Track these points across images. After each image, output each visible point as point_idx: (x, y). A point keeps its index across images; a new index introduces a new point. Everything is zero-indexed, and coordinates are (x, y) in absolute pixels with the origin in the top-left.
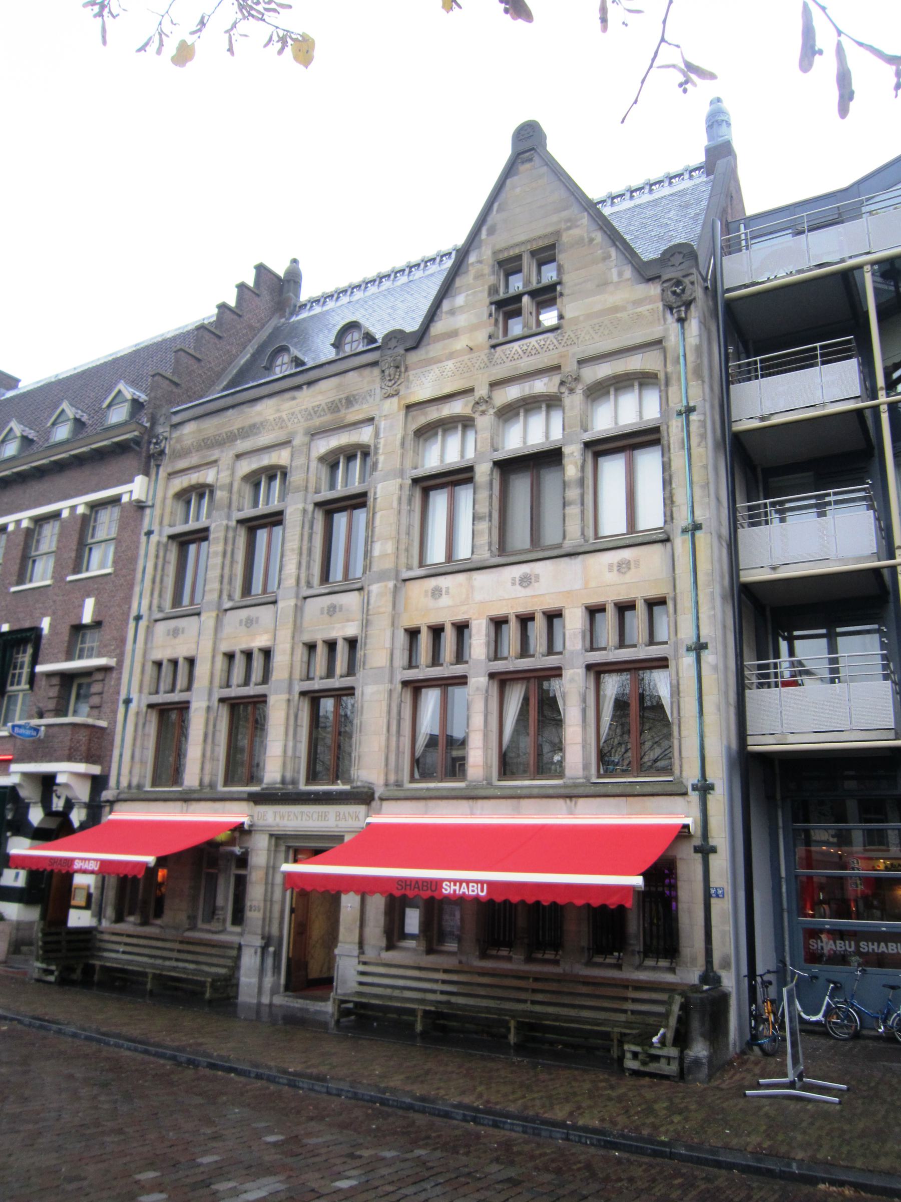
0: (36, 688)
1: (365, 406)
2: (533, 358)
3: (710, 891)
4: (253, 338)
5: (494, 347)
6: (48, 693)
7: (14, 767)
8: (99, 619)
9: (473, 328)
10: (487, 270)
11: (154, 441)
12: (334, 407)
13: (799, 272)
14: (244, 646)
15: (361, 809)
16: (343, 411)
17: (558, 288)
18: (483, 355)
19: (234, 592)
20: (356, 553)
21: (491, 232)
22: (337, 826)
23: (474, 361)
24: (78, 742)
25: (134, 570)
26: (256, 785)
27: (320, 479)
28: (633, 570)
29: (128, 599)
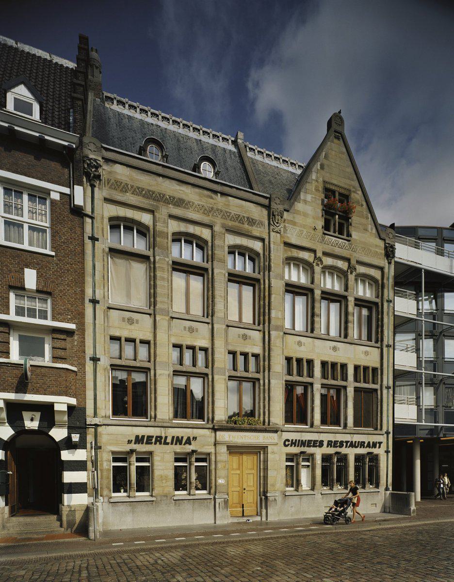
2: (340, 249)
10: (67, 65)
13: (408, 261)
20: (300, 322)
29: (81, 283)
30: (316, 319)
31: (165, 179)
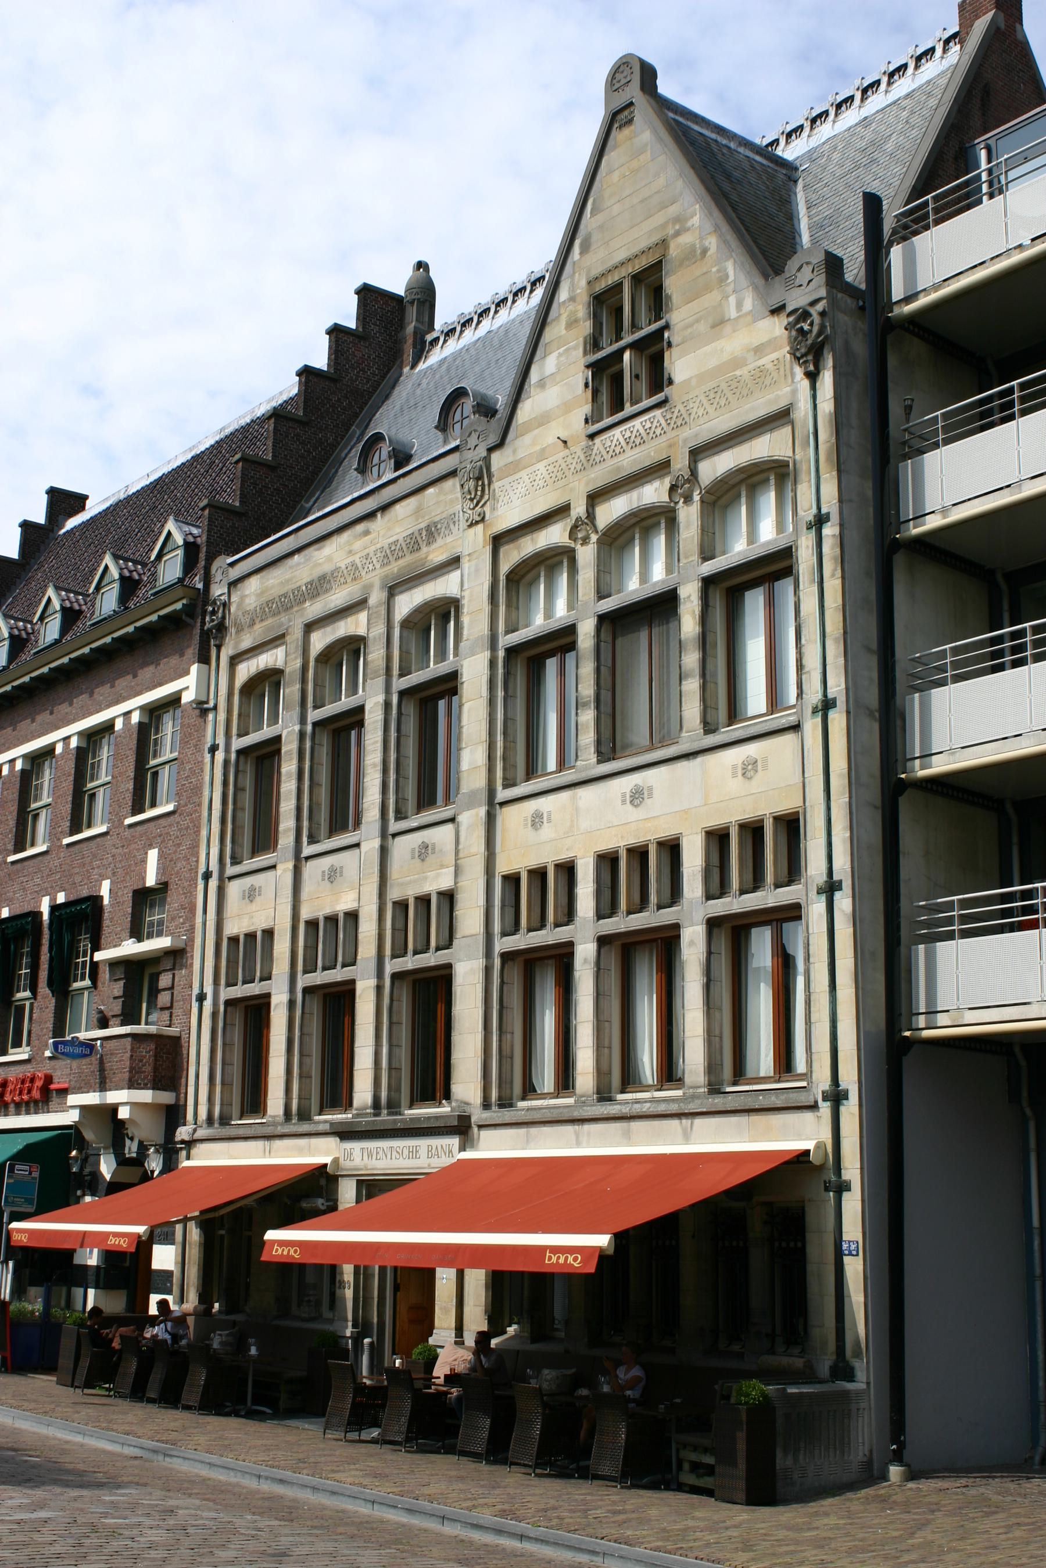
0: (100, 984)
1: (449, 539)
3: (841, 1246)
4: (361, 409)
5: (592, 436)
6: (113, 988)
7: (73, 1099)
8: (164, 879)
9: (567, 408)
11: (210, 609)
12: (414, 544)
14: (328, 911)
15: (454, 1141)
16: (425, 549)
17: (666, 335)
18: (578, 447)
19: (319, 829)
21: (585, 249)
22: (429, 1166)
23: (569, 460)
24: (141, 1061)
25: (200, 805)
26: (345, 1111)
27: (408, 653)
28: (760, 773)
30: (259, 1144)
31: (307, 552)
